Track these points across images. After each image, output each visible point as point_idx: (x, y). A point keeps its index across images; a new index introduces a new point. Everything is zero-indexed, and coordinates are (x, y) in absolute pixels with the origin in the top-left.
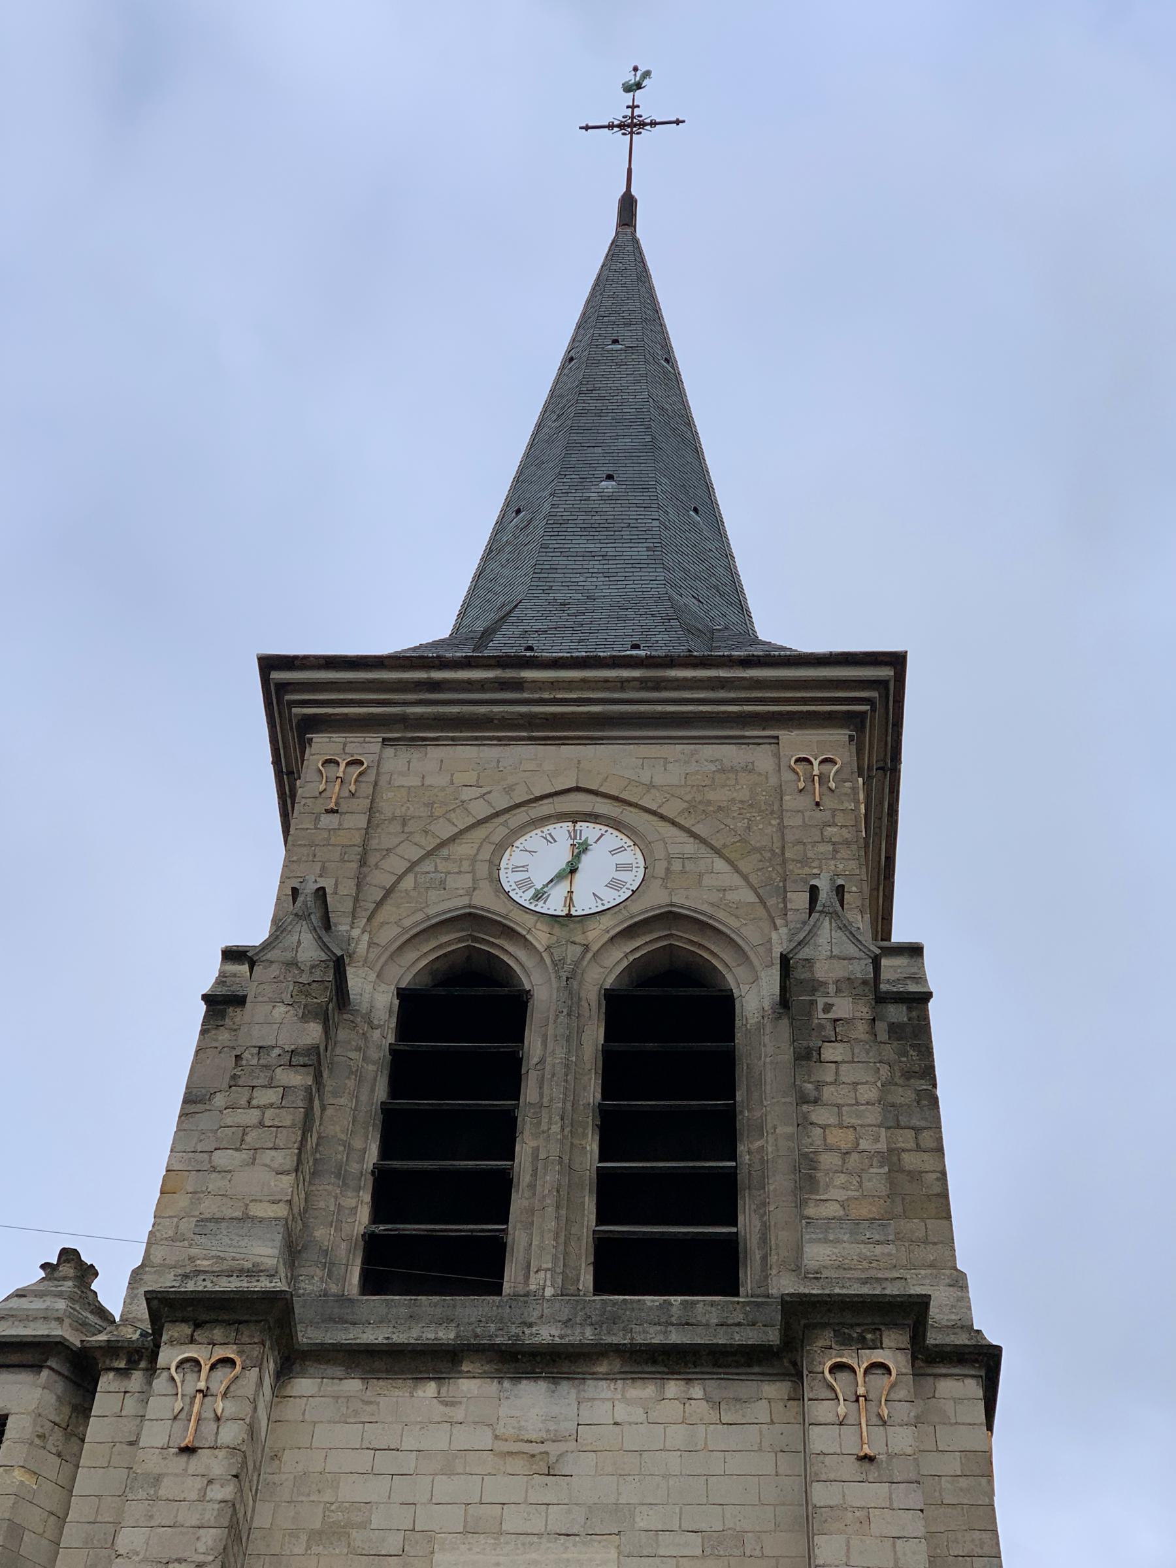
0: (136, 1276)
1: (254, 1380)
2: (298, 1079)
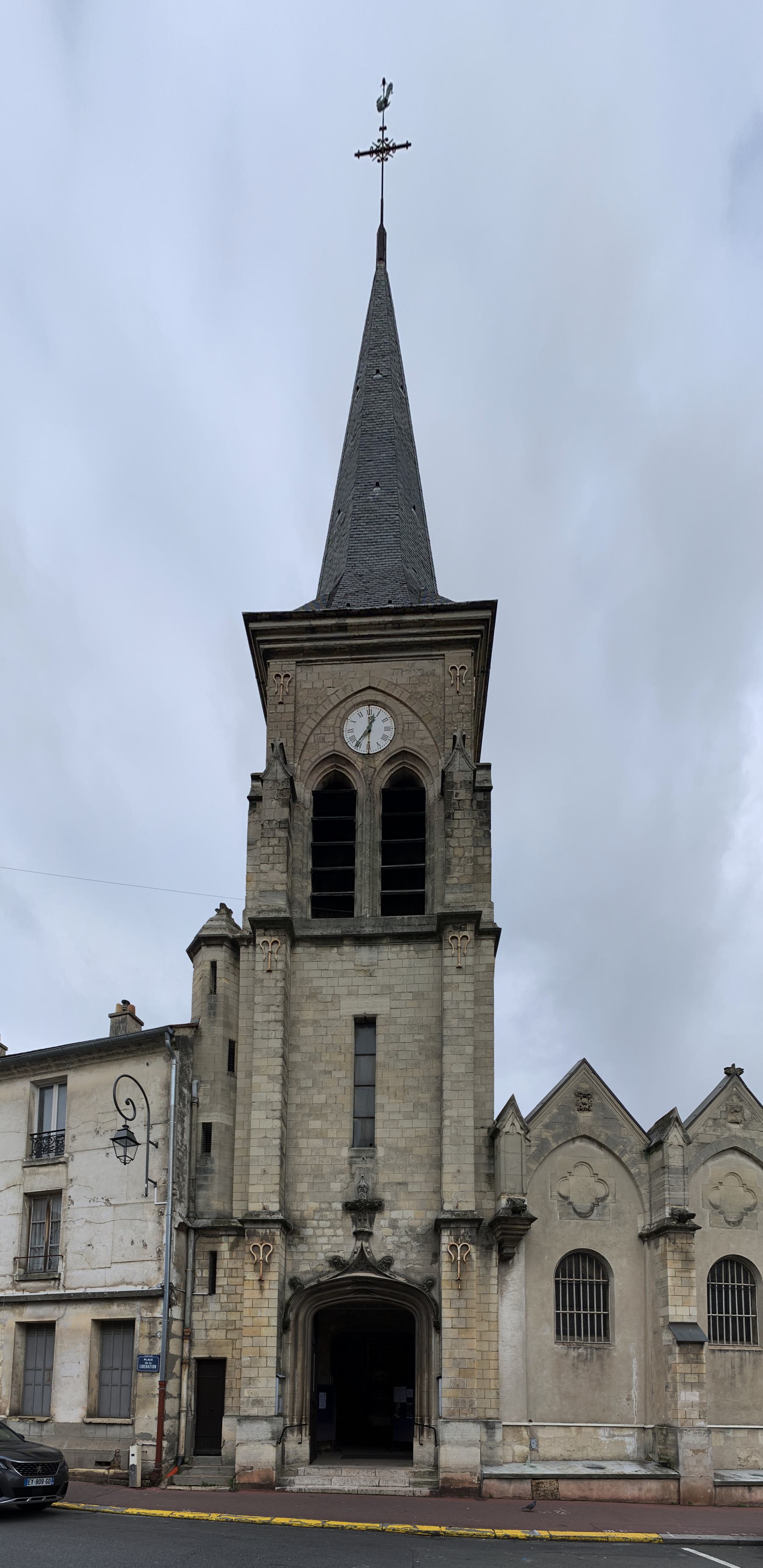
0: (244, 912)
1: (285, 948)
2: (282, 834)
